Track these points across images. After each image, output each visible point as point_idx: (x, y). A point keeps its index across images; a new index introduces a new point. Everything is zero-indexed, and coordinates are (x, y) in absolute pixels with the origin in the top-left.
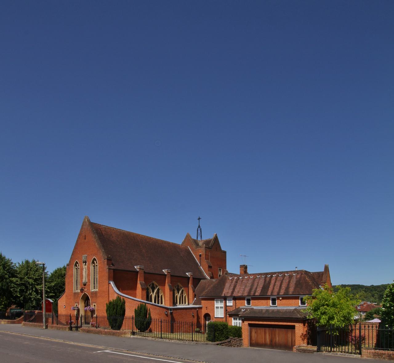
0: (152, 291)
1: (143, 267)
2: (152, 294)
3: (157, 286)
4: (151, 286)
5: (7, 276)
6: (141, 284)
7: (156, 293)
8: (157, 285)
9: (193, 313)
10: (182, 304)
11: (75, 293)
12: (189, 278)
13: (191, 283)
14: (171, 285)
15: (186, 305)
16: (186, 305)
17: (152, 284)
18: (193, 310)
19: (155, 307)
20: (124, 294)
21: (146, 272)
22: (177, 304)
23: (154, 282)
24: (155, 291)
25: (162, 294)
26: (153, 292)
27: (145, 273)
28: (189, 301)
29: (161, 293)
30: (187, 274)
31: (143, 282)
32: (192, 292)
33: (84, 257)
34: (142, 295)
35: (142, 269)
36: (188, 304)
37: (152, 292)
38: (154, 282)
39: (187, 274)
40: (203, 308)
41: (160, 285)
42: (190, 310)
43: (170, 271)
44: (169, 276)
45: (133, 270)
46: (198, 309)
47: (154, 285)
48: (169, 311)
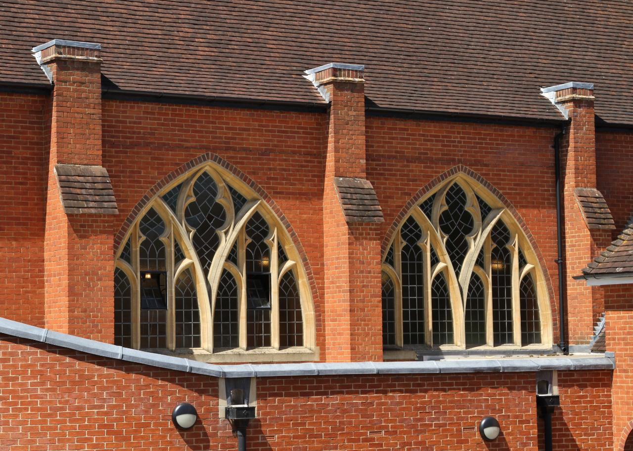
0: (449, 246)
1: (87, 50)
2: (189, 272)
3: (240, 202)
4: (440, 207)
5: (117, 210)
6: (347, 194)
7: (232, 257)
8: (490, 198)
9: (491, 423)
10: (498, 341)
12: (560, 127)
13: (578, 171)
14: (368, 185)
15: (541, 353)
16: (541, 353)
17: (443, 198)
18: (487, 395)
19: (78, 365)
20: (522, 295)
21: (382, 103)
22: (444, 348)
23: (209, 166)
24: (476, 244)
25: (527, 268)
26: (206, 248)
27: (372, 111)
28: (570, 318)
29: (523, 262)
30: (549, 94)
31: (99, 169)
32: (345, 238)
34: (71, 271)
35: (590, 104)
36: (563, 344)
37: (447, 258)
38: (461, 178)
39: (549, 94)
40: (618, 379)
41: (271, 190)
42: (460, 395)
43: (592, 91)
44: (357, 113)
45: (534, 113)
46: (562, 384)
47: (463, 199)
48: (223, 404)
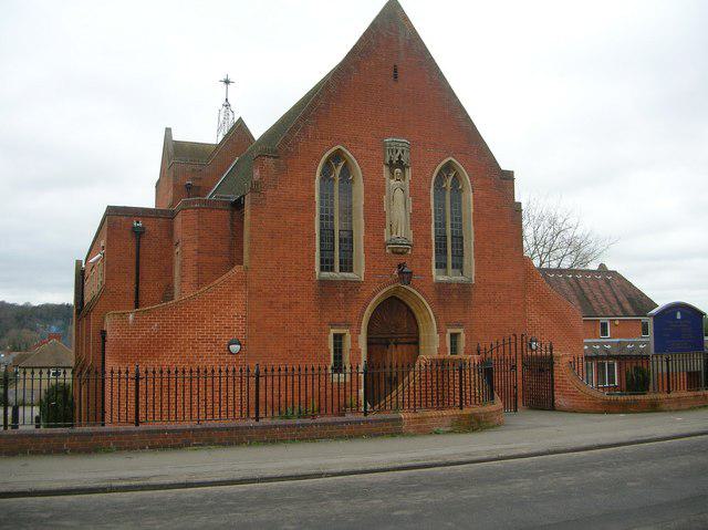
11: (323, 282)
33: (398, 142)
